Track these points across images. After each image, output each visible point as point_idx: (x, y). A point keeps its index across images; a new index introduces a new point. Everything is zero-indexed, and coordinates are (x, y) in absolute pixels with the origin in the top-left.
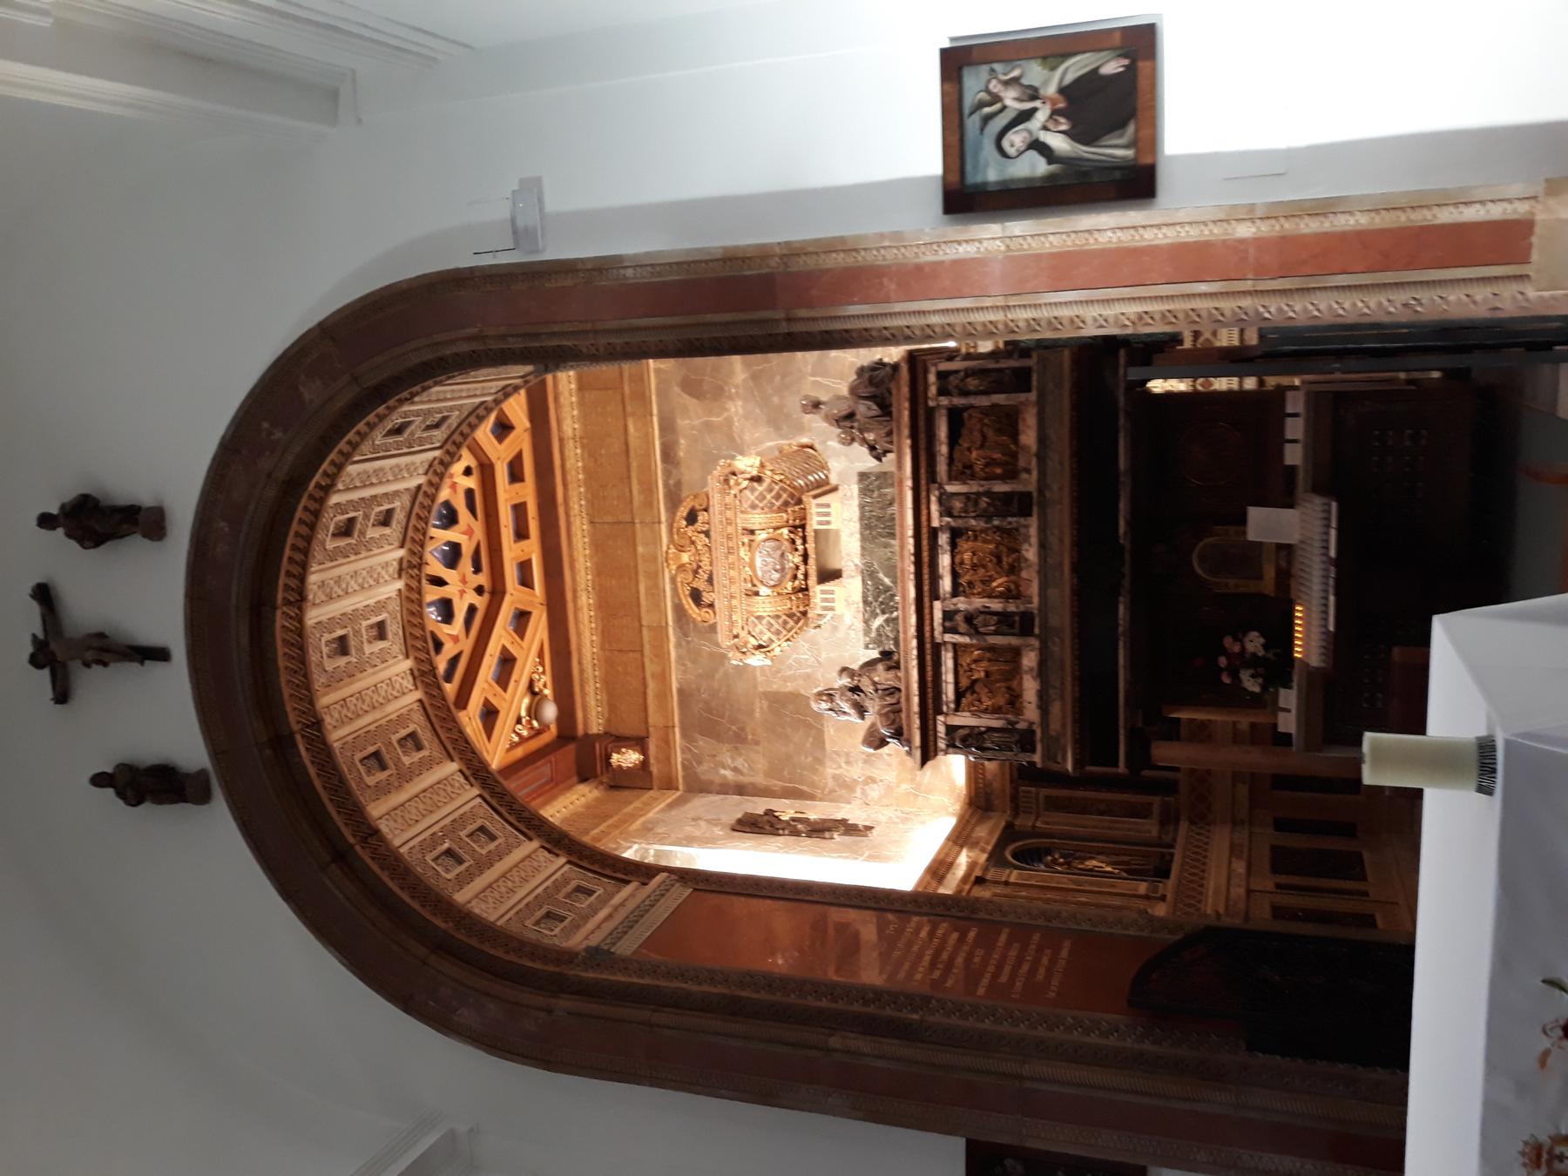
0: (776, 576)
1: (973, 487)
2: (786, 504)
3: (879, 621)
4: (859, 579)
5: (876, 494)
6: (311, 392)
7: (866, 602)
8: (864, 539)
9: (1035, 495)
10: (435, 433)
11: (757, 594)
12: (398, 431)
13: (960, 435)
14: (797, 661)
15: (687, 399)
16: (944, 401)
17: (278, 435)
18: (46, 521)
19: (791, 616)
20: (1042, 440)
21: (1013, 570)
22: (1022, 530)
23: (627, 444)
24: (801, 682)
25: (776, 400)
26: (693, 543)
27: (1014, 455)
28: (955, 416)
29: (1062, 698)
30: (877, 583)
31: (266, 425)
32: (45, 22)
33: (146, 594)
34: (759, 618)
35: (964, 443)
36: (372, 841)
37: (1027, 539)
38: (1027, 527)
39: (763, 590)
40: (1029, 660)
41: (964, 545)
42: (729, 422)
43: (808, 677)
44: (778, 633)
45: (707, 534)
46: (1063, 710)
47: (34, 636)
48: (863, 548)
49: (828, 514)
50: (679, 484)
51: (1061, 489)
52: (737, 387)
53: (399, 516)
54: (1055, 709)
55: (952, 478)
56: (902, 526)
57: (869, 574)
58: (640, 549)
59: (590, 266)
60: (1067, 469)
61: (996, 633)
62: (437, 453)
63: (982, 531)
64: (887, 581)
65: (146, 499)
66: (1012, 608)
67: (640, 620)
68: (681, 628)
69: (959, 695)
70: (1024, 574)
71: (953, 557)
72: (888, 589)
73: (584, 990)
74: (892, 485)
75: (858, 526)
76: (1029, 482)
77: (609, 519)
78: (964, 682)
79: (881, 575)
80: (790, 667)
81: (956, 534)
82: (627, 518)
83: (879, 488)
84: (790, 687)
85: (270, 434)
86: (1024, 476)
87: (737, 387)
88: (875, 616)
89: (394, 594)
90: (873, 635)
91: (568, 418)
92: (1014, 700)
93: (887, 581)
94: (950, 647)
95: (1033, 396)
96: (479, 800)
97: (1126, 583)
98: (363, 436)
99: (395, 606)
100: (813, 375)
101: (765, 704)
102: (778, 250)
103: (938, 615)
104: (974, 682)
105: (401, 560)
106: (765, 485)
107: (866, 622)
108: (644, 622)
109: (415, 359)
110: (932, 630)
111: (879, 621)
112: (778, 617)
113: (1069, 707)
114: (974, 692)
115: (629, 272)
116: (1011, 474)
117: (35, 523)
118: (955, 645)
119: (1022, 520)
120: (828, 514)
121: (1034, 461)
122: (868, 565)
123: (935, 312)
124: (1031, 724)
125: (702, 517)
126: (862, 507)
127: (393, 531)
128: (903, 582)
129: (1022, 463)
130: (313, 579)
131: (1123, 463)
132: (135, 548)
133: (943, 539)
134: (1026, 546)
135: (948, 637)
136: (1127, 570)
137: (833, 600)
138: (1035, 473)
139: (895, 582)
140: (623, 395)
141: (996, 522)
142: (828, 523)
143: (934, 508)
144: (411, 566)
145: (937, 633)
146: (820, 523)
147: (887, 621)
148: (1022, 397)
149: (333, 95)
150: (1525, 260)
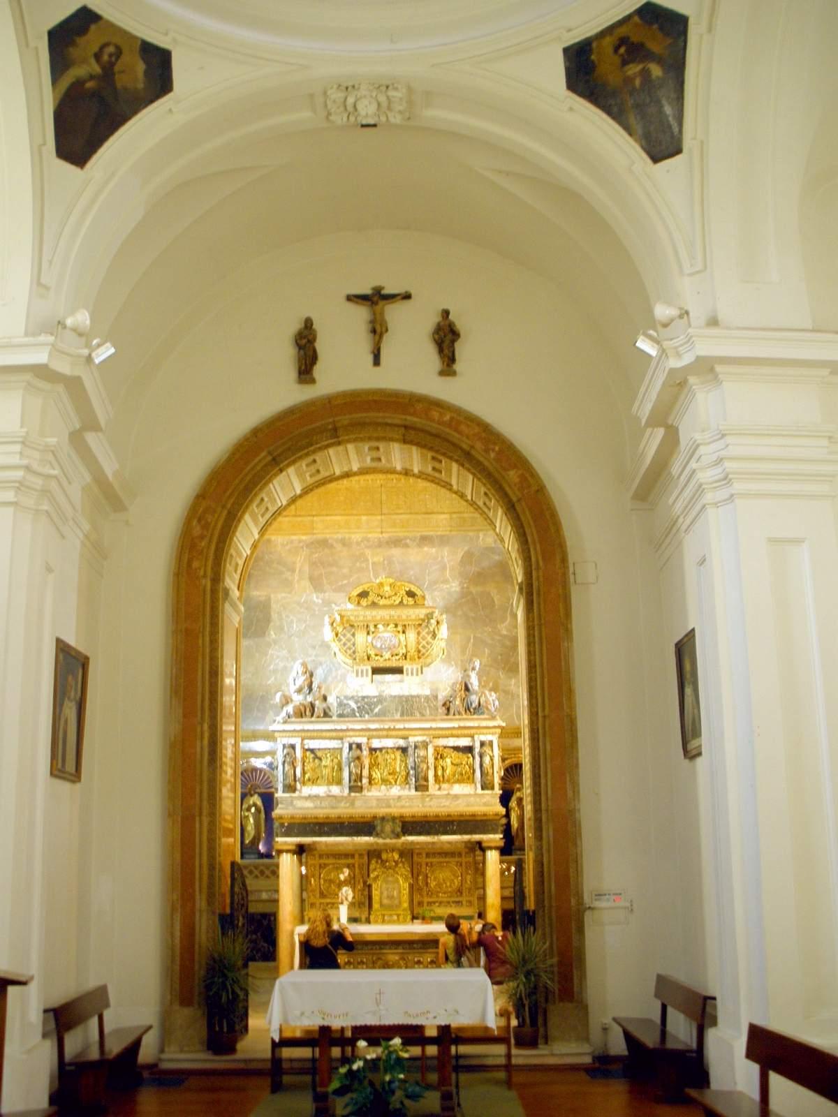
0: (379, 646)
1: (431, 760)
2: (419, 651)
3: (354, 705)
4: (377, 694)
5: (426, 704)
6: (513, 475)
7: (363, 698)
8: (400, 697)
9: (427, 793)
11: (368, 633)
13: (458, 751)
14: (292, 621)
17: (492, 455)
18: (446, 313)
19: (354, 652)
20: (456, 797)
21: (384, 781)
22: (407, 786)
23: (432, 513)
24: (278, 624)
25: (460, 613)
26: (396, 594)
27: (448, 781)
28: (469, 749)
29: (316, 808)
30: (376, 705)
31: (497, 448)
32: (671, 501)
33: (409, 368)
34: (353, 635)
35: (454, 754)
37: (403, 789)
39: (370, 638)
40: (335, 790)
41: (398, 754)
42: (446, 581)
43: (281, 629)
44: (345, 644)
46: (308, 808)
47: (383, 288)
48: (395, 697)
49: (412, 674)
50: (407, 546)
51: (430, 806)
54: (309, 804)
55: (436, 748)
56: (409, 721)
57: (380, 699)
58: (364, 518)
59: (569, 626)
60: (442, 810)
61: (350, 773)
63: (406, 764)
64: (376, 710)
65: (457, 367)
67: (316, 515)
68: (312, 543)
70: (383, 787)
72: (372, 710)
73: (214, 591)
74: (431, 714)
75: (406, 693)
77: (384, 497)
78: (319, 754)
79: (379, 707)
80: (287, 616)
81: (404, 750)
82: (385, 511)
83: (430, 707)
84: (274, 616)
85: (493, 450)
86: (437, 786)
88: (356, 702)
90: (345, 701)
92: (314, 781)
93: (376, 710)
94: (341, 746)
95: (479, 791)
96: (280, 505)
98: (485, 485)
100: (474, 637)
101: (262, 599)
102: (573, 713)
103: (358, 740)
104: (320, 759)
106: (431, 640)
107: (352, 698)
108: (315, 518)
109: (528, 531)
110: (351, 736)
111: (354, 705)
112: (354, 645)
113: (311, 811)
114: (314, 759)
115: (566, 644)
117: (445, 307)
118: (341, 749)
119: (413, 786)
120: (412, 674)
121: (446, 792)
122: (385, 699)
123: (547, 781)
124: (300, 791)
125: (411, 601)
126: (418, 696)
127: (429, 470)
128: (378, 721)
129: (444, 786)
130: (414, 448)
131: (445, 838)
132: (432, 359)
133: (402, 743)
135: (346, 745)
137: (362, 676)
138: (438, 793)
139: (376, 715)
140: (463, 512)
141: (412, 772)
142: (407, 674)
143: (420, 739)
145: (348, 739)
146: (407, 670)
147: (353, 710)
148: (479, 786)
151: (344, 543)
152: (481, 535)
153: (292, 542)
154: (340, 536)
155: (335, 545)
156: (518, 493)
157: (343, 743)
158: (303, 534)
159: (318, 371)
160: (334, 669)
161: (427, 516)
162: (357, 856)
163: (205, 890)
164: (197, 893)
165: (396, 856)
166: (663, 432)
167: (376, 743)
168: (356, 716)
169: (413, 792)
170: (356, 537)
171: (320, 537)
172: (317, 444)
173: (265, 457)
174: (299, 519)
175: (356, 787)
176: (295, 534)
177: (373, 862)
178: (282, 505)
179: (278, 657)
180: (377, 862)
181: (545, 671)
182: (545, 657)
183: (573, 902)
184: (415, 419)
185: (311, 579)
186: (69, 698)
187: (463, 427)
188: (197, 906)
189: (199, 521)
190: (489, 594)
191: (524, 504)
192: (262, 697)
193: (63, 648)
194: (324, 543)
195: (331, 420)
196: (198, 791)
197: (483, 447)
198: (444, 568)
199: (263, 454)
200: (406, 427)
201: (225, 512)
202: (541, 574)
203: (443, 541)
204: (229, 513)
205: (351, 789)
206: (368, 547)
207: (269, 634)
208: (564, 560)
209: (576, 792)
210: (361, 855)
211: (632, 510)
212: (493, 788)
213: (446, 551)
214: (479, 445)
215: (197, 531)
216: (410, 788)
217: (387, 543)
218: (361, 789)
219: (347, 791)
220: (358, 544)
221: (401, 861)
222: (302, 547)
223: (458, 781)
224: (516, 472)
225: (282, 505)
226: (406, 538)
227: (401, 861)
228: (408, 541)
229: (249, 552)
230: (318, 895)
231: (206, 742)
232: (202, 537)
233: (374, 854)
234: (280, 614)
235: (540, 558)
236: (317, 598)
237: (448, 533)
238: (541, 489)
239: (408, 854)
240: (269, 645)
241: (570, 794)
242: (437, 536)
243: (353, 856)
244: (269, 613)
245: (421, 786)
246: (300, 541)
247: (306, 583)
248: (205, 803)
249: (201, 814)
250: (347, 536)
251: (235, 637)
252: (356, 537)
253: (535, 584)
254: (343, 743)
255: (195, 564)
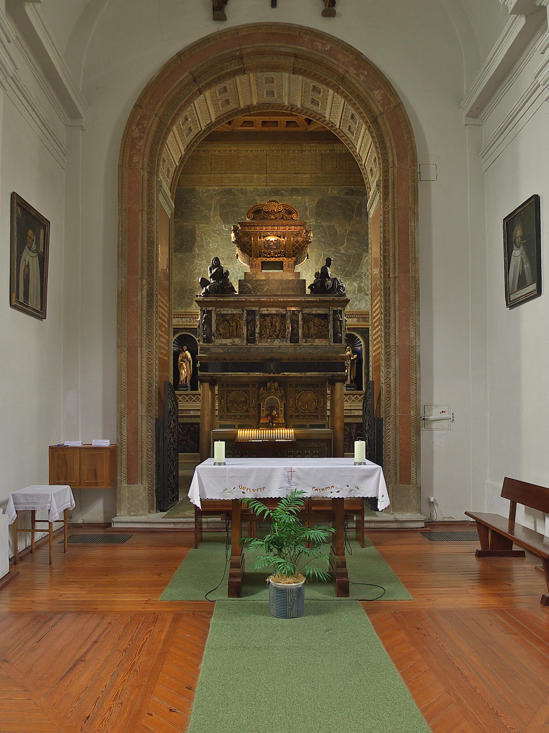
10: (347, 128)
12: (353, 117)
15: (316, 201)
16: (331, 313)
17: (362, 78)
20: (317, 347)
27: (311, 337)
28: (325, 317)
31: (366, 73)
35: (316, 320)
36: (198, 92)
37: (281, 341)
38: (286, 341)
43: (203, 246)
45: (282, 218)
50: (282, 195)
52: (320, 223)
53: (315, 108)
58: (255, 176)
62: (338, 127)
65: (338, 9)
66: (257, 335)
68: (222, 192)
69: (224, 315)
71: (274, 314)
76: (302, 342)
82: (269, 172)
84: (198, 239)
85: (363, 74)
86: (304, 340)
87: (320, 223)
89: (284, 101)
91: (238, 81)
97: (267, 375)
99: (279, 101)
101: (190, 227)
103: (254, 309)
105: (297, 106)
108: (224, 175)
109: (387, 139)
110: (248, 306)
116: (305, 336)
129: (309, 340)
131: (309, 374)
134: (279, 341)
136: (272, 375)
144: (292, 108)
148: (332, 340)
149: (476, 117)
150: (400, 483)
151: (242, 192)
152: (330, 188)
153: (209, 190)
154: (240, 188)
155: (237, 193)
156: (381, 109)
157: (243, 311)
158: (217, 186)
159: (229, 10)
160: (235, 273)
161: (295, 175)
162: (251, 386)
163: (145, 401)
164: (140, 404)
165: (276, 384)
166: (524, 22)
167: (264, 311)
168: (251, 293)
169: (289, 344)
170: (250, 188)
171: (227, 188)
172: (227, 69)
173: (187, 76)
174: (213, 176)
175: (251, 339)
176: (210, 186)
177: (262, 389)
178: (201, 130)
179: (200, 264)
180: (264, 389)
181: (397, 244)
182: (397, 233)
183: (412, 413)
184: (304, 49)
185: (221, 215)
186: (30, 248)
187: (340, 56)
188: (140, 413)
189: (137, 126)
190: (334, 227)
191: (384, 116)
192: (191, 289)
193: (18, 204)
194: (229, 192)
195: (238, 48)
196: (139, 329)
197: (355, 72)
198: (306, 209)
199: (186, 74)
200: (296, 56)
201: (157, 119)
202: (396, 170)
203: (305, 192)
204: (161, 121)
205: (248, 341)
206: (257, 195)
207: (195, 250)
208: (414, 160)
209: (418, 333)
210: (254, 385)
211: (466, 125)
212: (341, 342)
213: (307, 199)
214: (352, 70)
215: (136, 133)
216: (286, 340)
217: (270, 193)
218: (253, 341)
219: (245, 342)
220: (251, 193)
221: (280, 389)
222: (215, 195)
223: (318, 337)
224: (380, 92)
225: (201, 130)
226: (282, 189)
227: (280, 389)
228: (283, 192)
229: (177, 164)
230: (226, 411)
231: (145, 293)
232: (140, 138)
233: (262, 383)
234: (201, 237)
235: (396, 159)
236: (225, 227)
237: (309, 187)
238: (399, 105)
239: (283, 383)
240: (194, 257)
241: (412, 335)
242: (301, 189)
243: (248, 386)
244: (195, 237)
245: (294, 339)
246: (214, 190)
247: (218, 217)
248: (144, 337)
249: (141, 347)
250: (244, 188)
251: (168, 234)
252: (250, 188)
253: (391, 179)
254: (243, 311)
255: (135, 159)
